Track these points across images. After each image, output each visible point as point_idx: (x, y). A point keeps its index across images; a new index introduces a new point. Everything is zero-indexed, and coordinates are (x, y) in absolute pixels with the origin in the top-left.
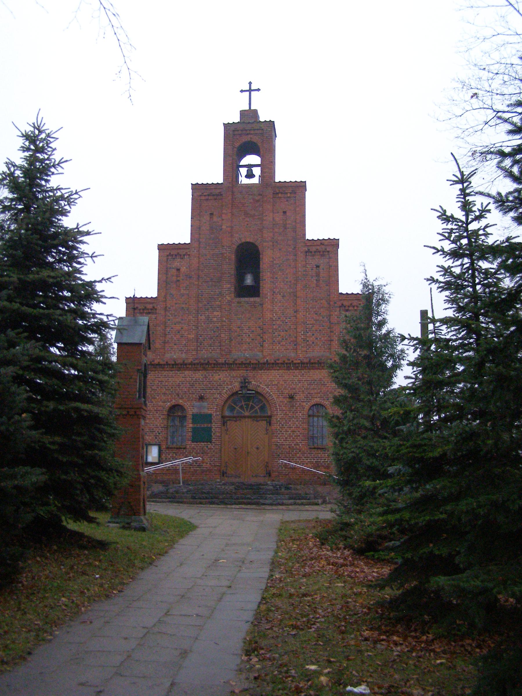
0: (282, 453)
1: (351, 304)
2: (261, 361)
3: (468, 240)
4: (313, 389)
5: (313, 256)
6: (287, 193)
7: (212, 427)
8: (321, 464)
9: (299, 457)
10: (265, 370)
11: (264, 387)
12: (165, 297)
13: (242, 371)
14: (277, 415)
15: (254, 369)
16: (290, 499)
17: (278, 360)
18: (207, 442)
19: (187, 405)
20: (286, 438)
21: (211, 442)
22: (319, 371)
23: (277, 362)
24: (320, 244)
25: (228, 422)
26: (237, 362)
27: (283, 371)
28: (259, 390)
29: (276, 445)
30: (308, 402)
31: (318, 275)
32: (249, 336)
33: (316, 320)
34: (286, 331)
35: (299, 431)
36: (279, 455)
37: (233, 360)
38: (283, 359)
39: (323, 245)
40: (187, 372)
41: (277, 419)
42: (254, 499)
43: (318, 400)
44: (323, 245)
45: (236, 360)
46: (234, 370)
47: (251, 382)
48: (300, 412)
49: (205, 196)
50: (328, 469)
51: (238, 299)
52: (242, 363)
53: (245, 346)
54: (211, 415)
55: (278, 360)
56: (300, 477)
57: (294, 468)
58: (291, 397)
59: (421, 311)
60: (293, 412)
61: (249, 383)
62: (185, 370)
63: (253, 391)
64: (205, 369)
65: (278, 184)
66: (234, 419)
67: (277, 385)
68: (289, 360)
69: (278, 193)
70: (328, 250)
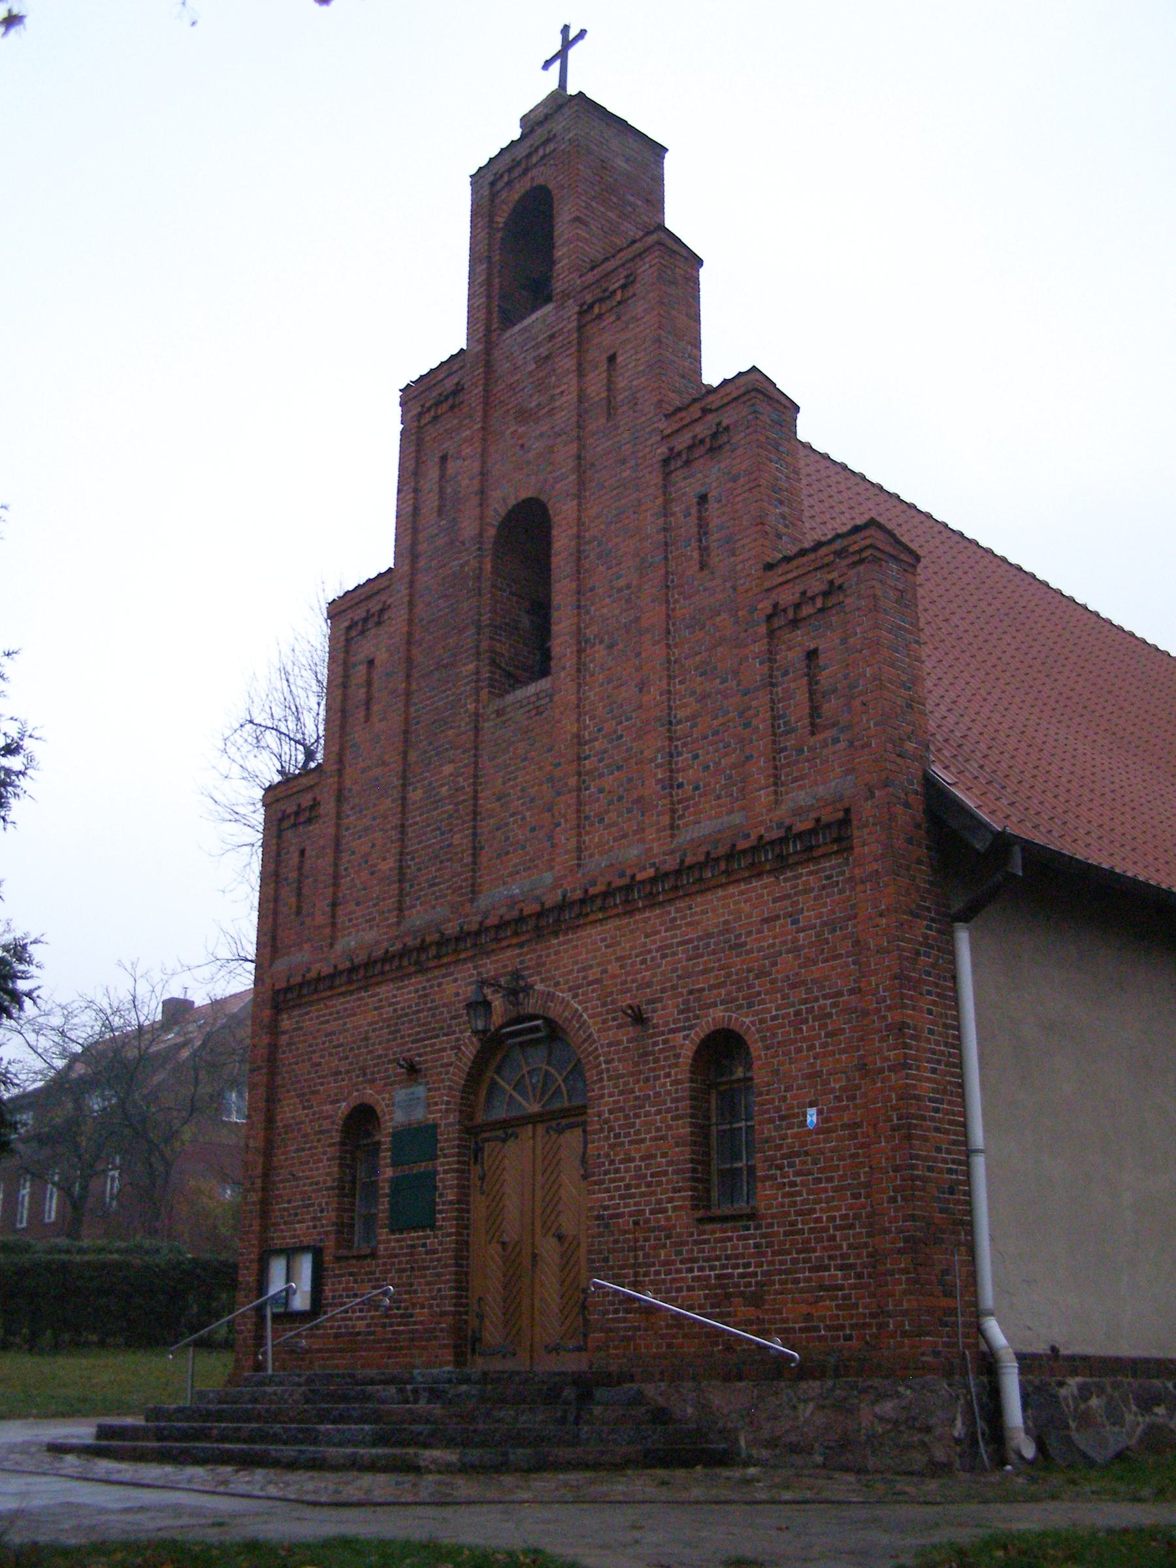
0: (615, 1251)
1: (804, 593)
4: (703, 972)
5: (688, 463)
6: (614, 292)
8: (737, 1285)
9: (666, 1263)
10: (566, 934)
11: (567, 996)
14: (602, 1096)
15: (539, 934)
16: (381, 1440)
18: (423, 1228)
20: (628, 1187)
22: (720, 893)
24: (699, 414)
26: (489, 922)
29: (598, 1217)
30: (691, 1028)
32: (523, 818)
33: (704, 697)
34: (619, 768)
35: (664, 1155)
36: (606, 1260)
37: (478, 918)
39: (711, 411)
40: (384, 991)
44: (711, 411)
45: (486, 916)
46: (488, 954)
47: (531, 987)
48: (668, 1075)
49: (429, 409)
50: (757, 1306)
52: (502, 925)
54: (435, 1126)
56: (669, 1346)
57: (651, 1310)
58: (638, 1018)
59: (666, 150)
60: (647, 1080)
62: (379, 984)
64: (422, 970)
65: (723, 391)
66: (500, 1133)
69: (591, 307)
70: (725, 423)
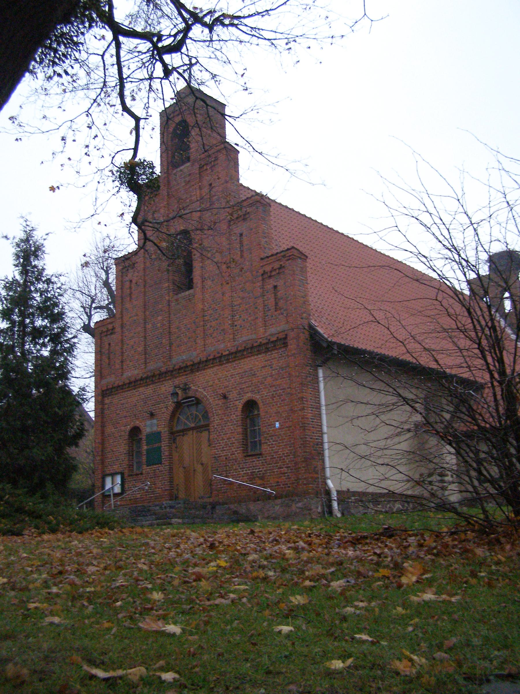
2: (196, 361)
3: (451, 418)
7: (161, 447)
9: (236, 469)
11: (202, 390)
12: (122, 312)
13: (183, 377)
15: (192, 371)
17: (209, 356)
18: (158, 464)
19: (141, 425)
21: (161, 463)
22: (249, 359)
23: (209, 358)
25: (178, 438)
27: (217, 368)
28: (198, 395)
31: (241, 243)
33: (243, 298)
38: (214, 354)
41: (213, 426)
42: (469, 456)
43: (249, 395)
46: (176, 377)
51: (176, 297)
53: (183, 348)
55: (209, 356)
57: (231, 483)
58: (225, 397)
61: (189, 388)
63: (191, 397)
64: (153, 383)
66: (182, 434)
67: (212, 386)
68: (219, 353)
